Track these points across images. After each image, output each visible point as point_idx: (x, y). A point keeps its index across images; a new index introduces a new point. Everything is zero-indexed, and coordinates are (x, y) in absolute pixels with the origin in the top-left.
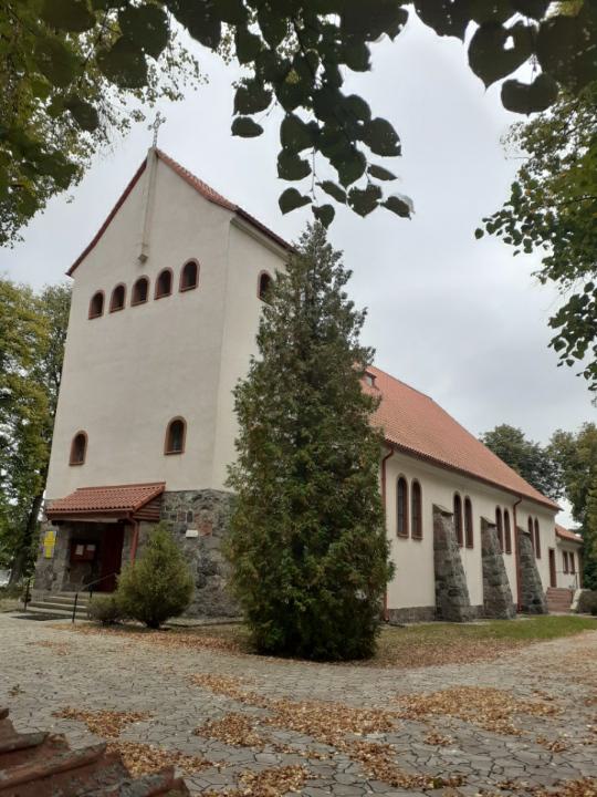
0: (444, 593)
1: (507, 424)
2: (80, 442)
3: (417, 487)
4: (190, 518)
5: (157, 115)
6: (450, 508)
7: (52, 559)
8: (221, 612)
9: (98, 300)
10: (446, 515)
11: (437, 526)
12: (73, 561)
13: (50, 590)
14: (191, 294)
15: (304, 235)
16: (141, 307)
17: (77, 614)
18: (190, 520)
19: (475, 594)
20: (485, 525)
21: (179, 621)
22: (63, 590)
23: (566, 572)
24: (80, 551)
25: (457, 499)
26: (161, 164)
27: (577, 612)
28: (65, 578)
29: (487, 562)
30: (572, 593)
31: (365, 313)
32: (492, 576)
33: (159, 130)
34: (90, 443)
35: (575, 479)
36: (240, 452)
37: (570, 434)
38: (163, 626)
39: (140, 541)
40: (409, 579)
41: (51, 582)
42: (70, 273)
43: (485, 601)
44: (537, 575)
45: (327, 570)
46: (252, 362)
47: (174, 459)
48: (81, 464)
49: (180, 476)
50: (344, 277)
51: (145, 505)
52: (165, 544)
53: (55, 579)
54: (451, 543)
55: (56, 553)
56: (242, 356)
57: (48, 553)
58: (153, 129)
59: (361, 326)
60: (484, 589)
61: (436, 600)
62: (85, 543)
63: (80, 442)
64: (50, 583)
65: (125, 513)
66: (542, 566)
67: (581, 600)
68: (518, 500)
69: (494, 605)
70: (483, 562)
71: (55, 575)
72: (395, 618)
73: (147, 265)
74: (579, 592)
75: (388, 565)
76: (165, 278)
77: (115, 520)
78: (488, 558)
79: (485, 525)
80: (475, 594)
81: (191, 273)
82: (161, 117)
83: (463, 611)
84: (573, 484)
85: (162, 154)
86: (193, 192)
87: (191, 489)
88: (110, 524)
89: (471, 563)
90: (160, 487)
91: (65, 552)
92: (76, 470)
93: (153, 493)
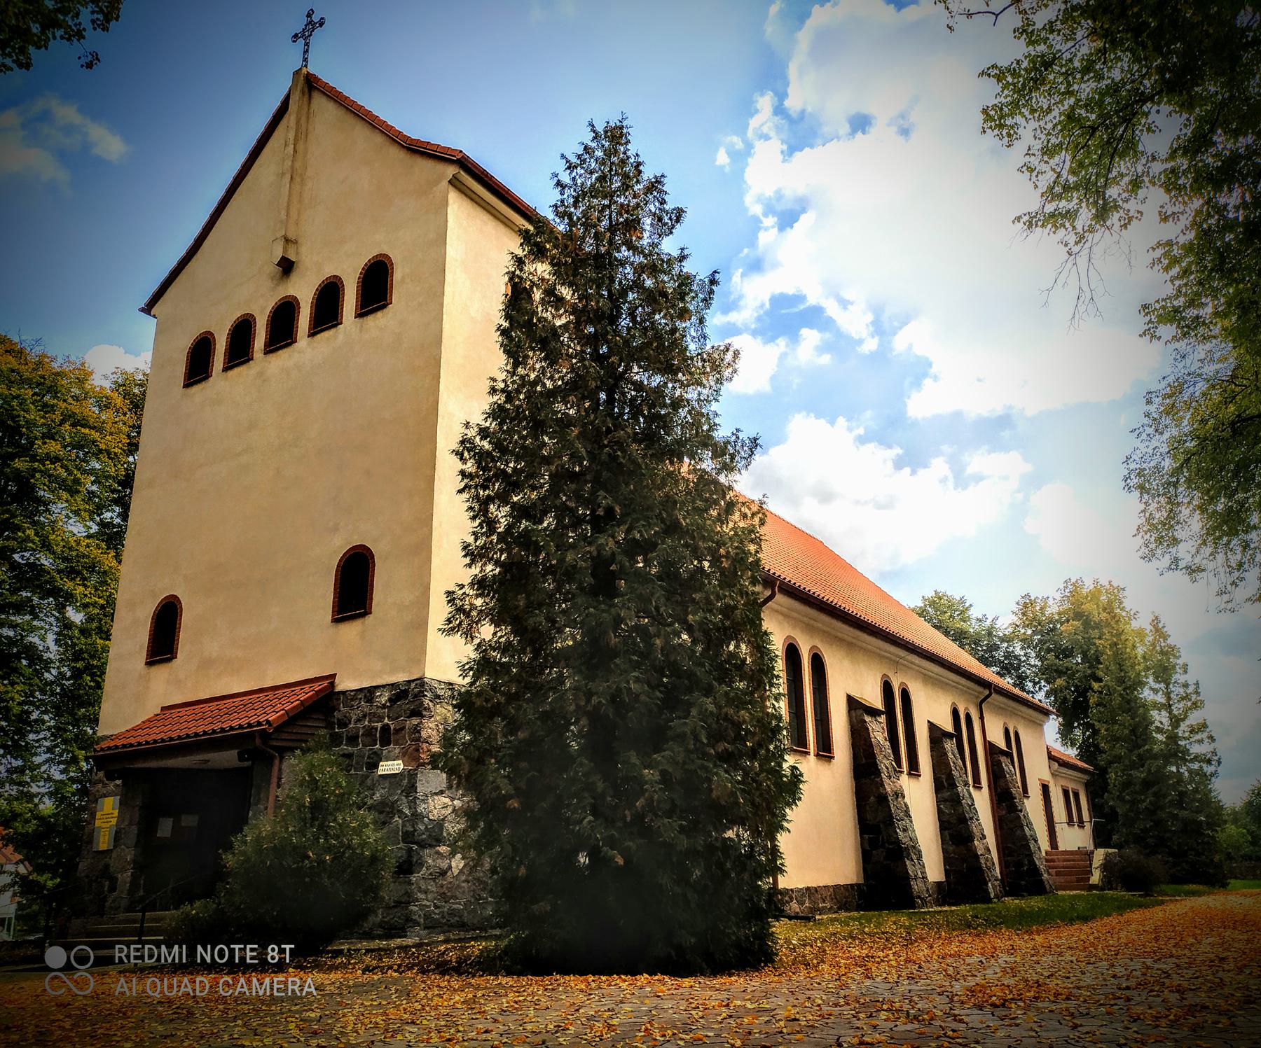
0: (879, 854)
1: (941, 589)
2: (167, 621)
3: (818, 664)
4: (386, 736)
5: (309, 15)
6: (877, 702)
8: (454, 920)
10: (874, 713)
11: (859, 735)
14: (378, 320)
15: (586, 149)
16: (284, 354)
18: (386, 741)
19: (931, 864)
20: (937, 735)
23: (1070, 822)
24: (165, 828)
25: (887, 689)
27: (1102, 889)
29: (945, 801)
30: (1089, 855)
31: (713, 282)
32: (955, 825)
34: (187, 618)
37: (1045, 599)
40: (814, 844)
42: (148, 309)
43: (947, 873)
44: (1030, 825)
46: (493, 391)
47: (351, 630)
48: (169, 660)
49: (358, 661)
50: (671, 220)
52: (73, 358)
54: (885, 762)
55: (118, 836)
56: (469, 381)
58: (301, 41)
59: (708, 306)
63: (167, 621)
65: (251, 736)
66: (1033, 807)
67: (1106, 866)
68: (768, 593)
69: (964, 879)
70: (938, 802)
72: (794, 906)
73: (294, 277)
74: (1099, 855)
75: (788, 772)
76: (329, 296)
78: (947, 794)
79: (937, 735)
80: (931, 864)
82: (316, 18)
83: (917, 886)
84: (1060, 682)
85: (317, 80)
86: (379, 139)
89: (917, 796)
92: (161, 673)
93: (305, 694)
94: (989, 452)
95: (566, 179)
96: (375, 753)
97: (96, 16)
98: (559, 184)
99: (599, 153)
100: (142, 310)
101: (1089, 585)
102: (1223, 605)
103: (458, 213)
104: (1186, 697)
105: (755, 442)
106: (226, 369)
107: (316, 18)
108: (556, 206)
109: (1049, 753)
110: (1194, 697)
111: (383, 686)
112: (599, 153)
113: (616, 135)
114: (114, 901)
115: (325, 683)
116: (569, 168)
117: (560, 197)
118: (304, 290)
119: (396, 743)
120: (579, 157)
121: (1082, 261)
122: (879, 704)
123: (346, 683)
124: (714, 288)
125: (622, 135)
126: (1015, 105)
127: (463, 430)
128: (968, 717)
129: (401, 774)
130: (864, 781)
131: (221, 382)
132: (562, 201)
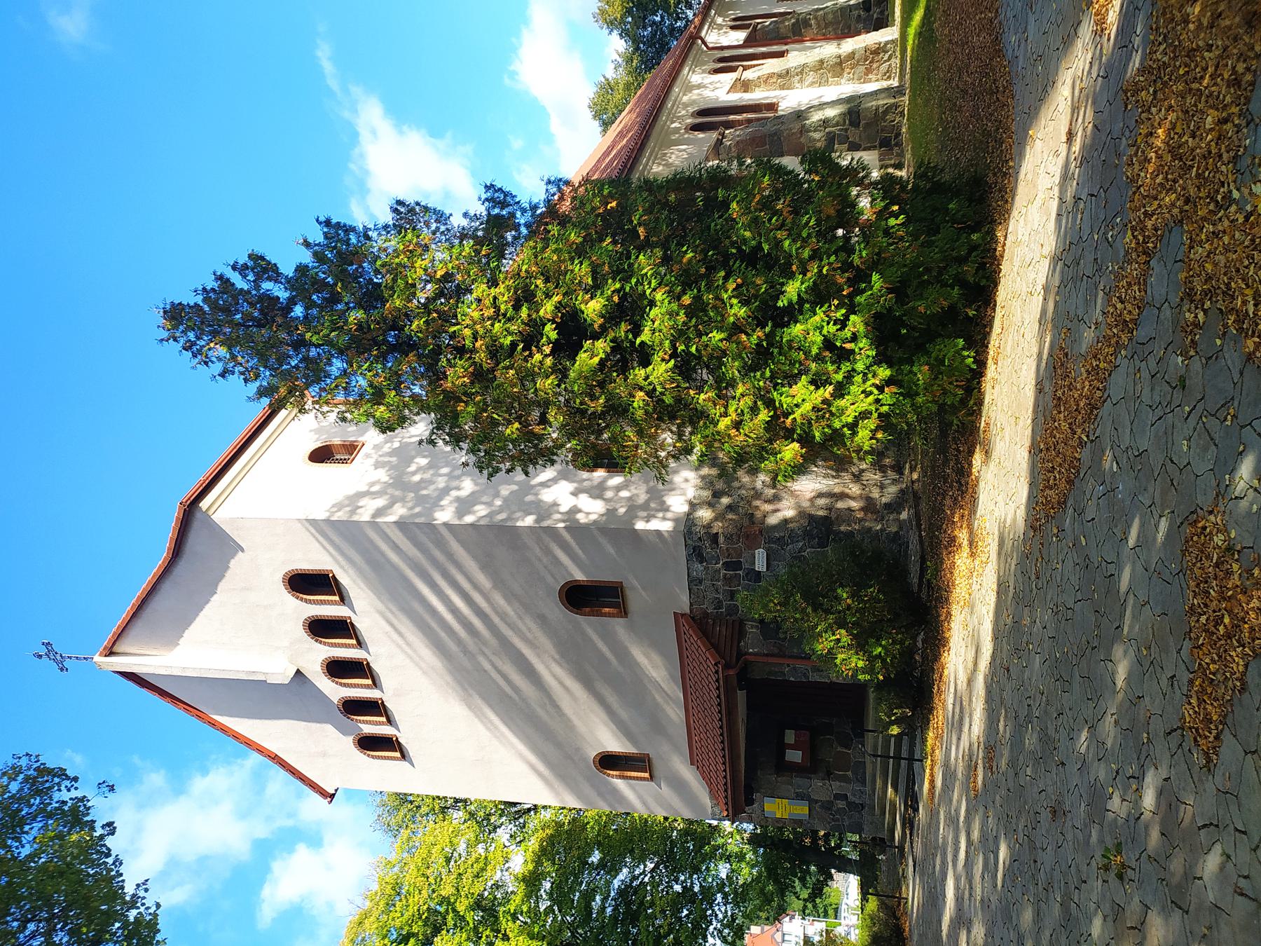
5: (40, 657)
7: (812, 802)
9: (369, 744)
12: (812, 767)
13: (863, 806)
17: (904, 754)
21: (914, 570)
22: (864, 783)
24: (794, 756)
28: (844, 779)
38: (924, 596)
39: (776, 651)
41: (850, 804)
46: (432, 442)
50: (261, 267)
51: (715, 647)
53: (845, 797)
55: (800, 797)
57: (802, 810)
59: (353, 229)
62: (782, 748)
64: (851, 805)
65: (726, 678)
71: (837, 797)
76: (321, 628)
77: (741, 696)
81: (306, 583)
86: (166, 586)
88: (750, 706)
90: (682, 621)
91: (798, 781)
93: (695, 641)
94: (178, 787)
97: (63, 788)
98: (223, 375)
99: (191, 336)
108: (246, 380)
109: (404, 756)
113: (175, 314)
114: (854, 795)
116: (206, 363)
119: (740, 555)
120: (195, 356)
122: (714, 135)
123: (683, 602)
129: (767, 550)
130: (785, 148)
132: (242, 373)
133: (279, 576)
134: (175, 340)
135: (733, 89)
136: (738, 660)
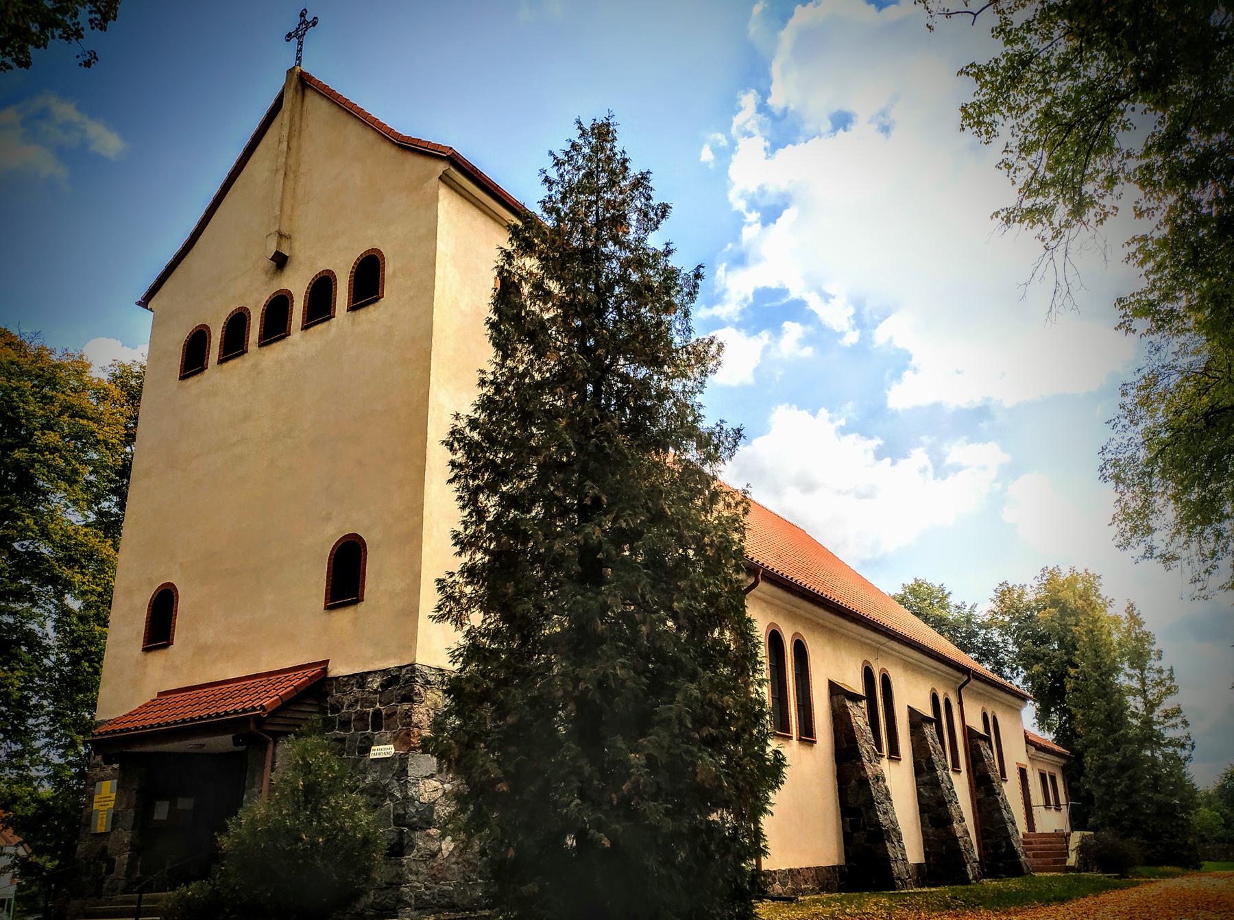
0: (860, 837)
1: (921, 577)
2: (163, 608)
4: (378, 721)
5: (302, 15)
6: (858, 688)
8: (444, 901)
10: (855, 698)
11: (840, 720)
14: (370, 314)
15: (574, 145)
18: (377, 726)
19: (911, 847)
20: (917, 720)
23: (1047, 805)
24: (162, 811)
25: (868, 674)
26: (311, 97)
27: (1079, 871)
29: (925, 784)
30: (1066, 838)
31: (698, 276)
32: (934, 808)
33: (298, 20)
34: (183, 606)
35: (1037, 659)
36: (465, 558)
37: (1023, 587)
42: (145, 303)
43: (927, 855)
44: (1007, 808)
45: (651, 762)
46: (483, 383)
47: (344, 617)
48: (165, 646)
49: (350, 648)
50: (657, 215)
54: (866, 747)
58: (295, 40)
59: (692, 300)
60: (924, 833)
61: (846, 851)
63: (163, 608)
65: (245, 720)
66: (1010, 791)
69: (943, 860)
72: (777, 887)
73: (288, 271)
74: (1076, 838)
76: (322, 290)
78: (926, 778)
79: (917, 720)
80: (911, 847)
82: (309, 18)
83: (897, 868)
84: (1037, 668)
86: (371, 136)
87: (375, 668)
89: (898, 780)
92: (157, 659)
94: (968, 443)
95: (554, 175)
96: (367, 738)
97: (93, 16)
98: (547, 180)
99: (586, 150)
100: (139, 304)
101: (1065, 573)
102: (1197, 593)
103: (449, 208)
104: (1160, 683)
105: (738, 433)
106: (221, 361)
107: (309, 18)
108: (544, 202)
110: (1168, 683)
111: (375, 672)
112: (586, 150)
113: (603, 132)
114: (111, 883)
115: (318, 669)
116: (556, 164)
117: (548, 193)
118: (297, 284)
119: (388, 728)
120: (567, 153)
121: (1059, 255)
122: (860, 689)
123: (338, 669)
124: (699, 282)
125: (608, 132)
126: (993, 103)
127: (453, 421)
128: (947, 702)
129: (392, 758)
130: (845, 765)
131: (216, 374)
132: (550, 197)
133: (377, 244)
134: (582, 135)
135: (912, 712)
136: (271, 733)
